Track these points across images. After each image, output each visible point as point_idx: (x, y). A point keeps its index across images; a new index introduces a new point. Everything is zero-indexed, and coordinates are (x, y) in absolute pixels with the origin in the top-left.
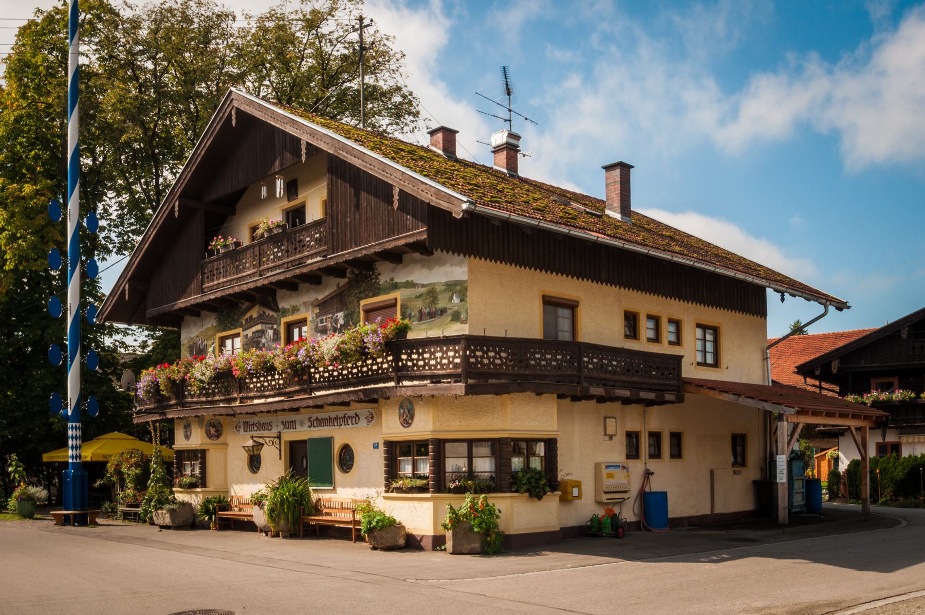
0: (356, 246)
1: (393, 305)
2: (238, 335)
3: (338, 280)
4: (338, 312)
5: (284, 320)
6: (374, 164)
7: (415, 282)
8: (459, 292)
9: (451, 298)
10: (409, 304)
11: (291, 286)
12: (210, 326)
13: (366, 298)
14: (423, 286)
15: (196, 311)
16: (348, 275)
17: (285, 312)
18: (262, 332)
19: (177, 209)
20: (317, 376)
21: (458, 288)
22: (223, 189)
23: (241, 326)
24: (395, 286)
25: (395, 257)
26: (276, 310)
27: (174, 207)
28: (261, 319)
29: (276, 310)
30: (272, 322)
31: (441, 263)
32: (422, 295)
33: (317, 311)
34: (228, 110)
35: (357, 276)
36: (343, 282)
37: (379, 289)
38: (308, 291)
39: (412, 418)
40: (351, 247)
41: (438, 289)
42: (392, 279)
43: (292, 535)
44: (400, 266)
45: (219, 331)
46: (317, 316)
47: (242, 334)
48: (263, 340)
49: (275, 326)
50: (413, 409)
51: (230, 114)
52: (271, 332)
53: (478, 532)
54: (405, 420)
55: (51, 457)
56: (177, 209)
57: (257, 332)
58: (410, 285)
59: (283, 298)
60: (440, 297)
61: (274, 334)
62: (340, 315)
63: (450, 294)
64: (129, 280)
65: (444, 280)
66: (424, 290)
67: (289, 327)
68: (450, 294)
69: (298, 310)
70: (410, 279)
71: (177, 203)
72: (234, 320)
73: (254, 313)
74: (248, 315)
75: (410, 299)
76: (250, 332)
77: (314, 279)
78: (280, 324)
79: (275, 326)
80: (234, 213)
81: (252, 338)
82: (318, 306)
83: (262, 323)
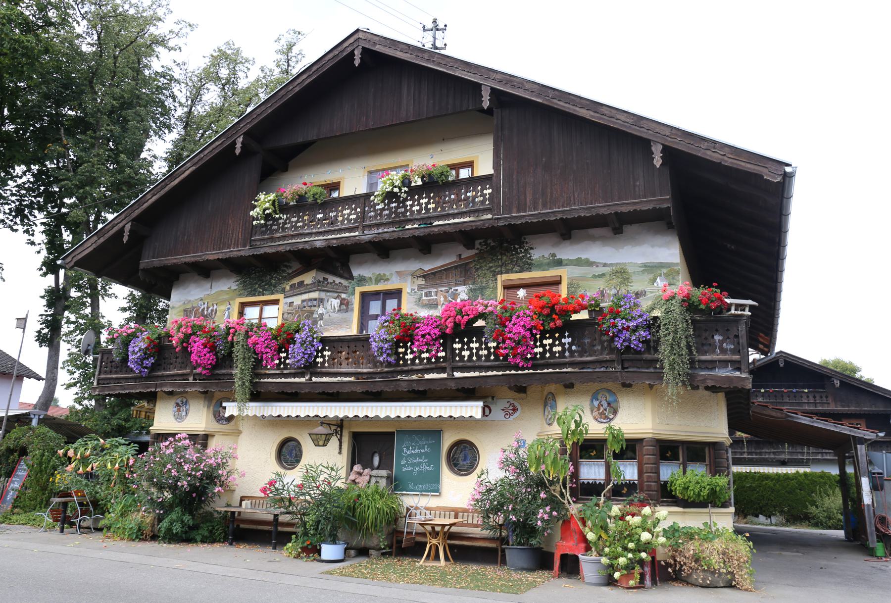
0: (545, 206)
1: (557, 282)
2: (276, 302)
3: (461, 249)
4: (460, 285)
5: (359, 290)
6: (618, 116)
7: (591, 260)
8: (667, 275)
9: (654, 280)
10: (581, 283)
11: (384, 250)
12: (225, 288)
13: (507, 272)
14: (605, 265)
15: (205, 271)
16: (477, 245)
17: (362, 280)
18: (321, 301)
19: (239, 145)
20: (466, 353)
21: (665, 271)
22: (287, 140)
23: (283, 291)
24: (559, 263)
25: (568, 229)
26: (351, 277)
27: (234, 143)
28: (319, 285)
29: (351, 277)
30: (336, 290)
31: (633, 240)
32: (603, 275)
33: (421, 281)
34: (349, 50)
35: (493, 248)
36: (467, 253)
37: (530, 264)
38: (406, 258)
39: (615, 412)
40: (535, 209)
41: (630, 270)
42: (554, 255)
43: (184, 537)
44: (567, 242)
45: (240, 295)
46: (420, 288)
47: (283, 301)
48: (321, 310)
49: (343, 296)
50: (616, 401)
51: (352, 54)
52: (336, 302)
53: (622, 576)
54: (601, 414)
55: (872, 534)
56: (239, 145)
57: (311, 300)
58: (589, 263)
59: (361, 264)
60: (633, 278)
61: (341, 304)
62: (461, 289)
63: (651, 276)
64: (133, 220)
65: (641, 260)
66: (607, 270)
67: (366, 298)
68: (651, 276)
69: (388, 279)
70: (583, 257)
71: (241, 139)
72: (271, 285)
73: (308, 278)
74: (296, 280)
75: (584, 278)
76: (297, 300)
77: (425, 245)
78: (353, 293)
79: (343, 296)
80: (285, 169)
81: (301, 308)
82: (424, 276)
83: (320, 290)
